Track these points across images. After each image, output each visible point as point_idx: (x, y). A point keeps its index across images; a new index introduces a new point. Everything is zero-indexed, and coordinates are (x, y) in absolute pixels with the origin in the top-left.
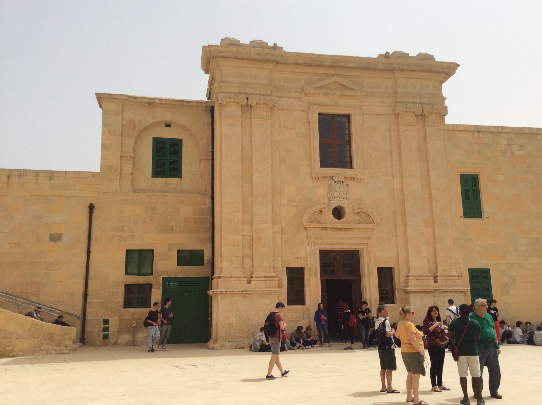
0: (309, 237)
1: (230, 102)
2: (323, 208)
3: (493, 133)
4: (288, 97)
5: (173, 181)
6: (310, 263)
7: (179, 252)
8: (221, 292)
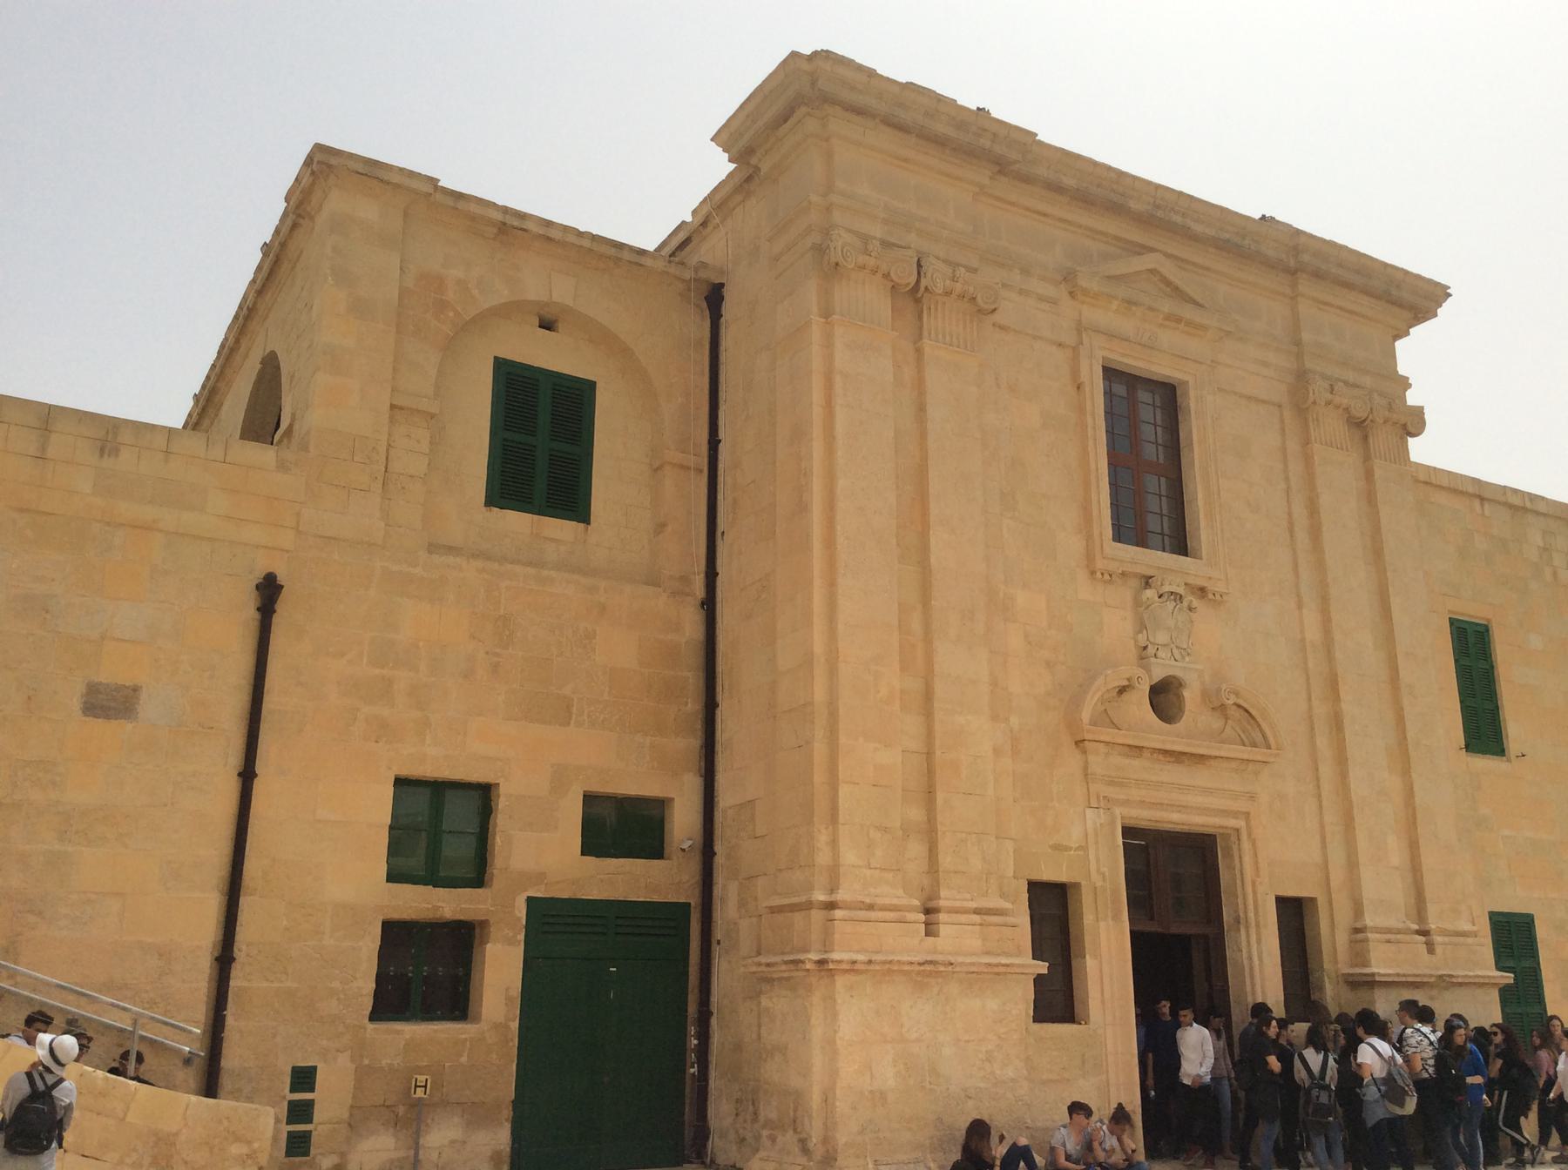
0: (1091, 774)
1: (863, 267)
2: (1139, 677)
3: (1511, 507)
4: (1021, 292)
5: (560, 529)
6: (1098, 870)
7: (590, 799)
8: (854, 962)
